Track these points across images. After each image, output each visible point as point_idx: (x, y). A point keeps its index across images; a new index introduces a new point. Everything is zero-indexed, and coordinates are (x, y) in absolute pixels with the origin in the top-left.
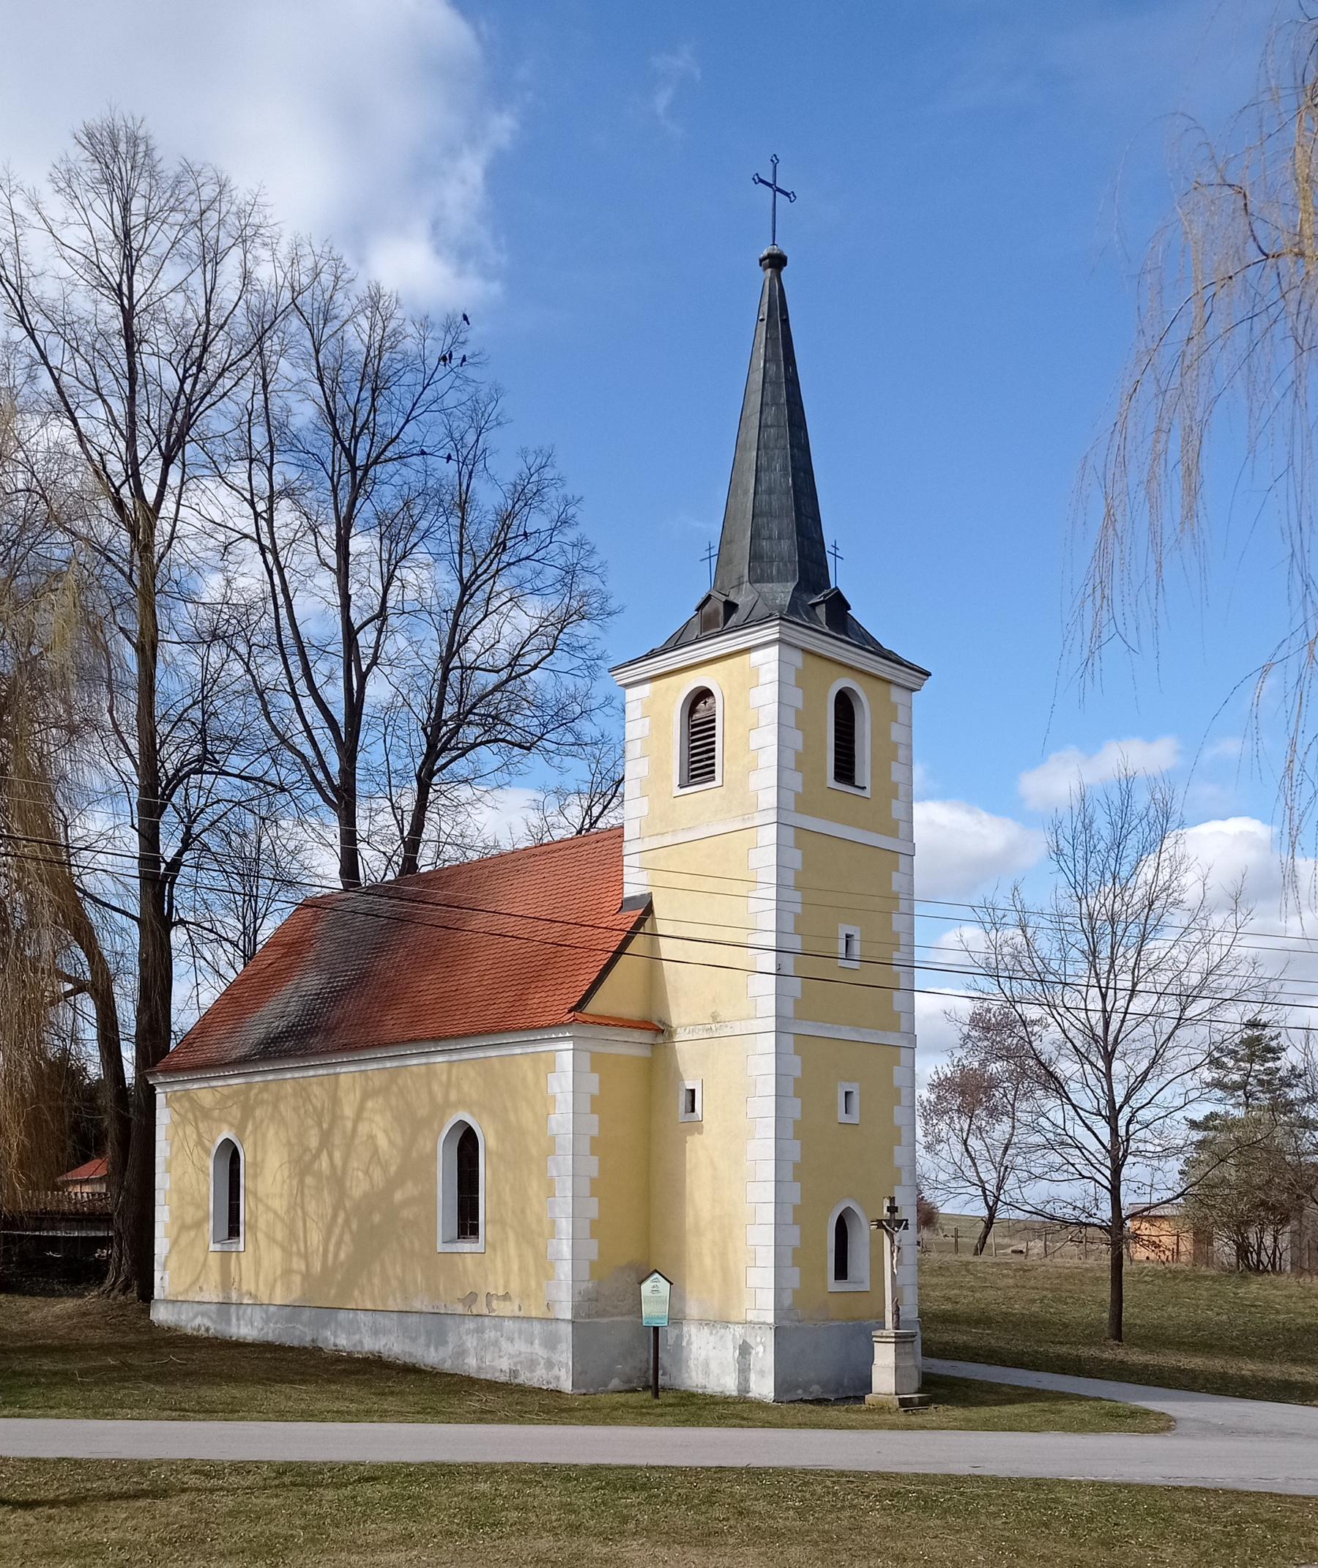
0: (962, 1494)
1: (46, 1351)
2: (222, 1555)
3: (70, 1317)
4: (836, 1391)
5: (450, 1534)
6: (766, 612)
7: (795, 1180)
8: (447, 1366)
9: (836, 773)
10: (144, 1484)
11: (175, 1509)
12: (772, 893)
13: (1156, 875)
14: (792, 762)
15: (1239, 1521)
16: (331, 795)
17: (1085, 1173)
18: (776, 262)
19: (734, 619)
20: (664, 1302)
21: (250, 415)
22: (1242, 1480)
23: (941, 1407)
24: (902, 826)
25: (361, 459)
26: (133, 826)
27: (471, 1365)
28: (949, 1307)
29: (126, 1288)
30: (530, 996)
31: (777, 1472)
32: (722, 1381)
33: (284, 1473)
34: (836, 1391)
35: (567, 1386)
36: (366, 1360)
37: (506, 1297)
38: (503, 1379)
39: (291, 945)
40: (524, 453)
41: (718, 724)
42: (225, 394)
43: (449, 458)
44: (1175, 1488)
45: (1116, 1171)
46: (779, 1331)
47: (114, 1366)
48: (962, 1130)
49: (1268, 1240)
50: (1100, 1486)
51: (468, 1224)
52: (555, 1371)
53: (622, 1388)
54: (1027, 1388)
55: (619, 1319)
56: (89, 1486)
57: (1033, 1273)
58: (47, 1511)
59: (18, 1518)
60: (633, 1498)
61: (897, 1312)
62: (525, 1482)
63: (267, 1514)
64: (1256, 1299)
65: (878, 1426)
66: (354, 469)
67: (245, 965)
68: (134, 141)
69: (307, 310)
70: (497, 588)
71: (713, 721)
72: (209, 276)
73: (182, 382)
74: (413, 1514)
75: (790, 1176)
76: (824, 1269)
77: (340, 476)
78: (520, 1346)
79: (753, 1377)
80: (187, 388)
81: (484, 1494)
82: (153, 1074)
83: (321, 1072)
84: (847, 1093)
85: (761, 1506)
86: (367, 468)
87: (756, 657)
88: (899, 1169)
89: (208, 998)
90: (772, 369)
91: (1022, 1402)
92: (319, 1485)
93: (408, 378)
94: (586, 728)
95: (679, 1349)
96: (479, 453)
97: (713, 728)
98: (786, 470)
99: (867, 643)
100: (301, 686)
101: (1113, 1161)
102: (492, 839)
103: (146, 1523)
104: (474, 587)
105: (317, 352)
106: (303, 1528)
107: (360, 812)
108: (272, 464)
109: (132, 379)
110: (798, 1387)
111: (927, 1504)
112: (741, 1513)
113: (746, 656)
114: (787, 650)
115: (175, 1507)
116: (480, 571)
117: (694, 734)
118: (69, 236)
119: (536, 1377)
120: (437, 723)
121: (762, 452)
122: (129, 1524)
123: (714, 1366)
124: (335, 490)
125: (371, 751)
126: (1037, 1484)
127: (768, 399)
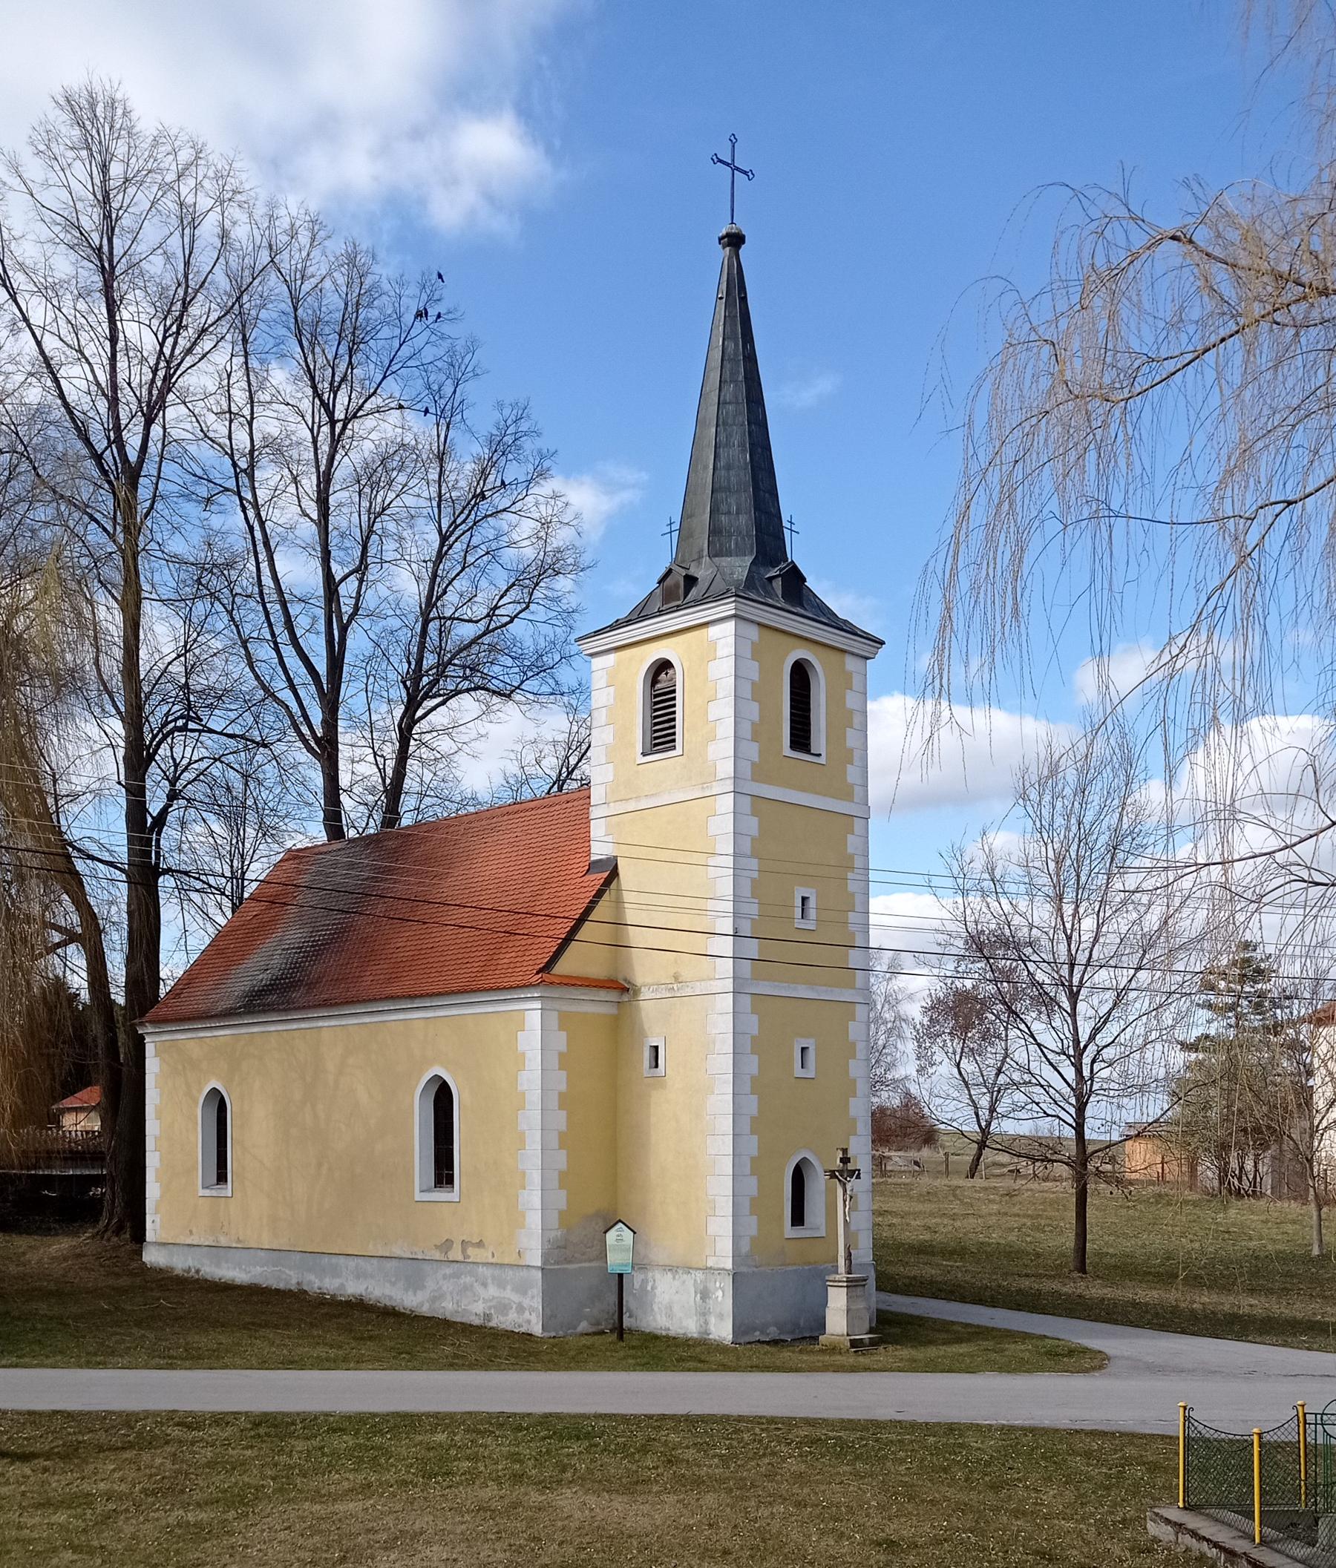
0: (877, 1440)
1: (46, 1295)
2: (199, 1505)
3: (65, 1259)
4: (793, 1332)
5: (404, 1483)
6: (723, 587)
7: (752, 1133)
8: (425, 1310)
9: (792, 742)
10: (131, 1433)
11: (158, 1461)
12: (729, 861)
13: (1120, 819)
14: (749, 733)
15: (1127, 1461)
16: (313, 744)
17: (1049, 1112)
18: (734, 241)
19: (694, 593)
20: (628, 1250)
21: (229, 376)
22: (1144, 1422)
23: (890, 1348)
24: (857, 790)
25: (339, 414)
26: (119, 783)
27: (448, 1308)
28: (927, 1236)
29: (118, 1231)
30: (501, 956)
31: (704, 1419)
32: (685, 1324)
33: (259, 1424)
34: (793, 1332)
35: (537, 1330)
36: (348, 1304)
37: (480, 1244)
38: (477, 1322)
39: (276, 895)
40: (500, 406)
41: (678, 694)
42: (204, 356)
43: (426, 411)
44: (1077, 1431)
45: (1081, 1108)
46: (736, 1277)
47: (108, 1311)
48: (954, 1053)
49: (1249, 1165)
50: (1007, 1430)
51: (444, 1173)
52: (527, 1314)
53: (591, 1331)
54: (978, 1326)
55: (587, 1265)
56: (80, 1438)
57: (1019, 1198)
58: (43, 1463)
59: (16, 1470)
60: (576, 1447)
61: (849, 1257)
62: (479, 1432)
63: (242, 1465)
64: (1234, 1225)
65: (825, 1368)
66: (333, 422)
67: (233, 912)
68: (112, 104)
69: (285, 266)
70: (475, 541)
71: (674, 691)
72: (187, 240)
73: (162, 345)
74: (375, 1465)
75: (747, 1129)
76: (781, 1217)
77: (319, 427)
78: (492, 1291)
79: (712, 1320)
80: (167, 351)
81: (440, 1445)
82: (142, 1024)
83: (303, 1025)
84: (803, 1049)
85: (690, 1454)
86: (346, 422)
87: (714, 631)
88: (854, 1120)
89: (200, 940)
90: (731, 346)
91: (969, 1340)
92: (291, 1435)
93: (386, 332)
94: (566, 675)
95: (645, 1296)
96: (456, 405)
97: (674, 698)
98: (744, 446)
99: (824, 615)
100: (283, 637)
101: (1077, 1100)
102: (469, 791)
103: (131, 1474)
104: (452, 539)
105: (296, 310)
106: (273, 1479)
107: (342, 765)
108: (252, 418)
109: (113, 340)
110: (755, 1329)
111: (842, 1450)
112: (669, 1461)
113: (704, 631)
114: (743, 625)
115: (159, 1459)
116: (459, 521)
117: (656, 703)
118: (48, 198)
119: (508, 1321)
120: (418, 673)
121: (721, 428)
122: (116, 1475)
123: (676, 1308)
124: (315, 441)
125: (352, 695)
126: (951, 1428)
127: (727, 375)
